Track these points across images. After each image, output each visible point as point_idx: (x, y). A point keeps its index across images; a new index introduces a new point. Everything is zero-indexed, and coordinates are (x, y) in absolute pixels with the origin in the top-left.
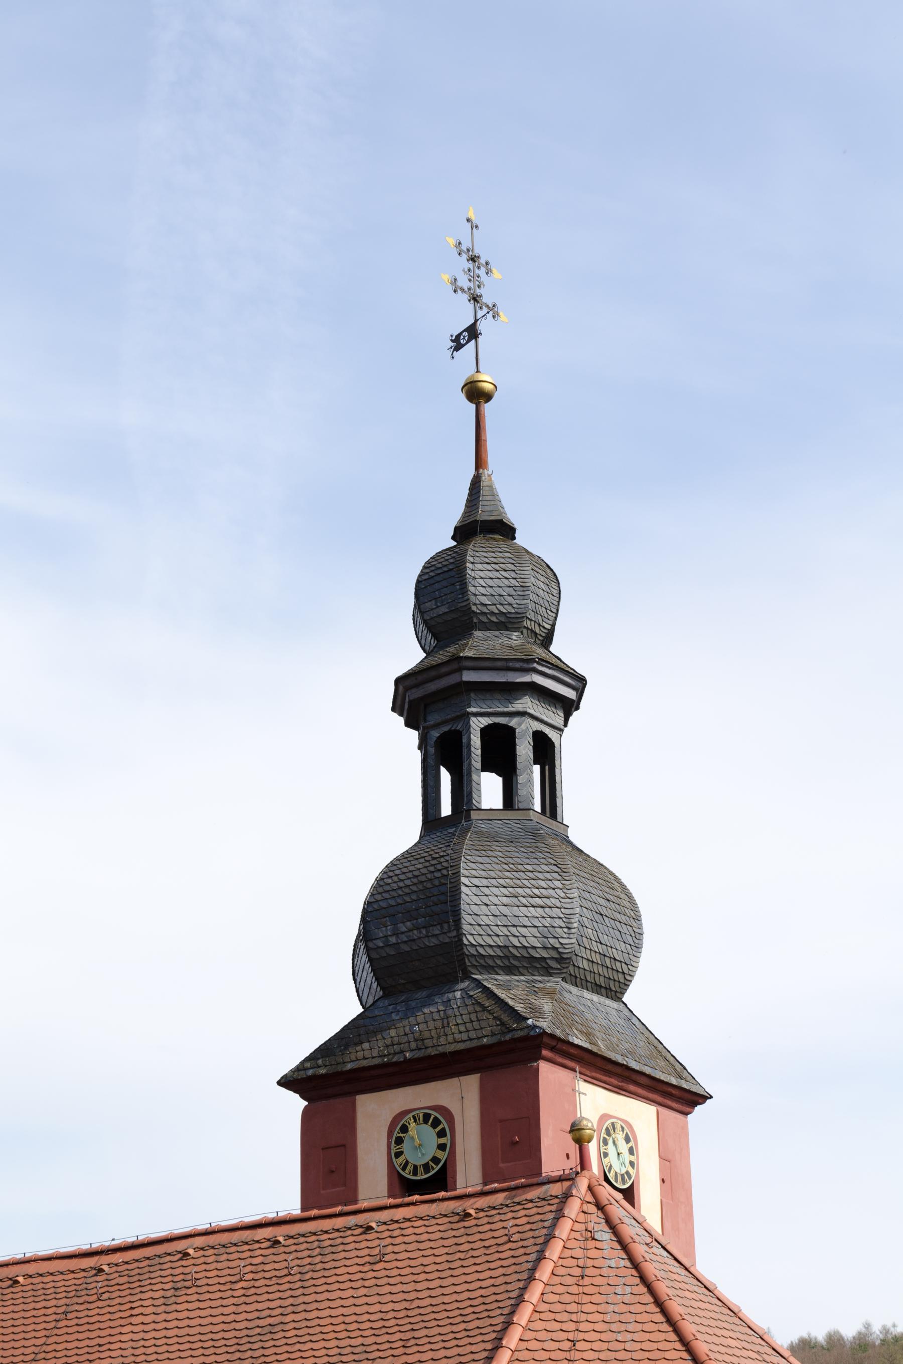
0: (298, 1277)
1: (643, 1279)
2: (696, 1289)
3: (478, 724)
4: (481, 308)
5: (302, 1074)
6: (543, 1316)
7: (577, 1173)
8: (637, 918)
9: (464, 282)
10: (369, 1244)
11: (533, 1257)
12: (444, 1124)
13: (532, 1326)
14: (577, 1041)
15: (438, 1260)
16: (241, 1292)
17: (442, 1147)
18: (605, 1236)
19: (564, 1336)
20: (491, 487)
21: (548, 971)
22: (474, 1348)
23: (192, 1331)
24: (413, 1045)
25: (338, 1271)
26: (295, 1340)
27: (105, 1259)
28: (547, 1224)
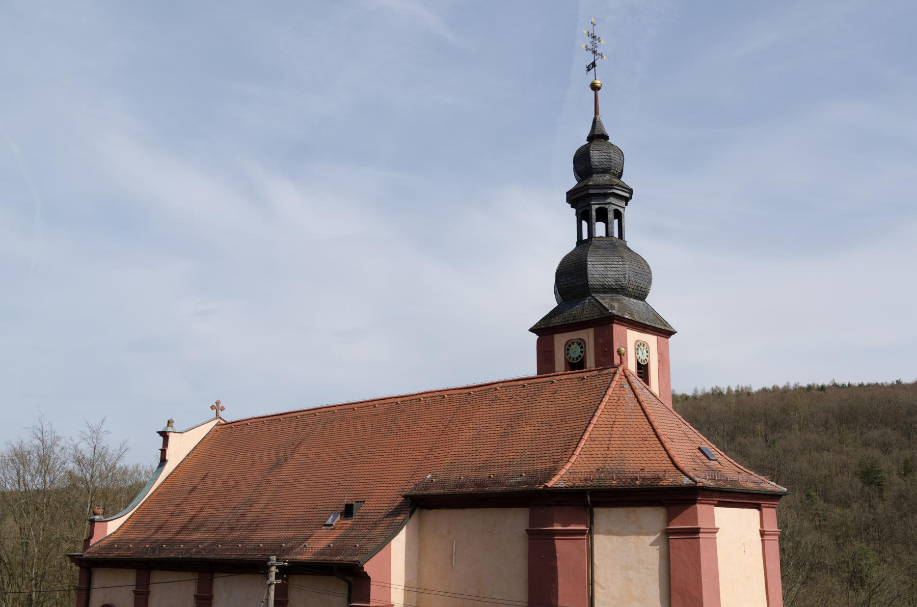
0: (530, 397)
1: (639, 401)
2: (657, 403)
3: (594, 207)
4: (597, 55)
5: (536, 328)
6: (605, 413)
7: (619, 365)
8: (650, 273)
9: (590, 47)
10: (553, 387)
11: (603, 393)
12: (583, 344)
13: (601, 416)
14: (626, 317)
15: (574, 393)
16: (513, 402)
17: (582, 352)
18: (627, 386)
19: (611, 420)
20: (600, 122)
21: (618, 293)
22: (583, 423)
23: (497, 414)
24: (572, 318)
25: (543, 396)
26: (528, 418)
27: (472, 390)
28: (608, 382)
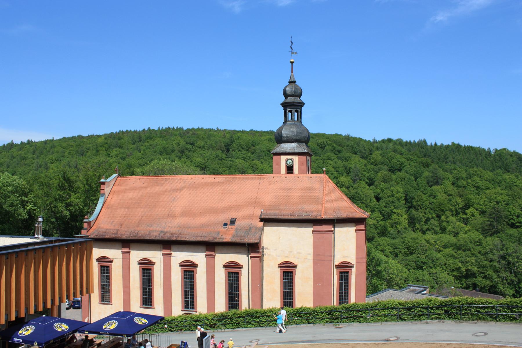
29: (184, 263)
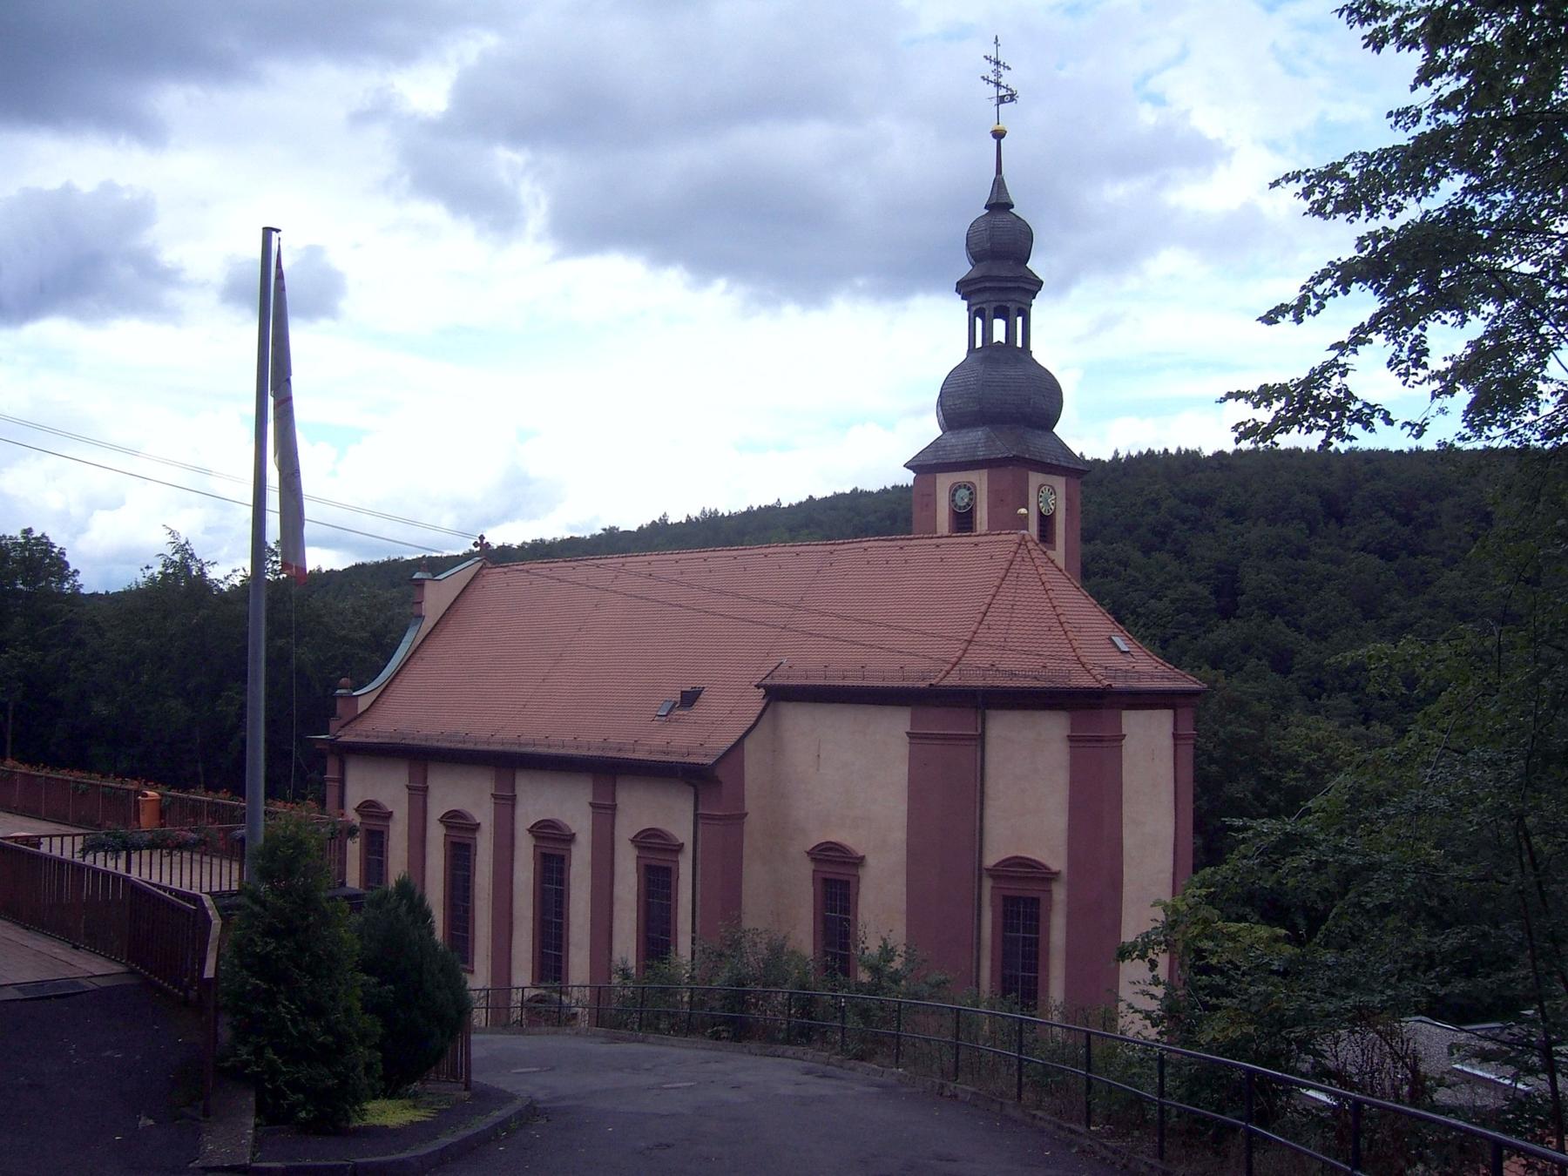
5: (915, 464)
9: (992, 78)
17: (971, 499)
29: (644, 838)
